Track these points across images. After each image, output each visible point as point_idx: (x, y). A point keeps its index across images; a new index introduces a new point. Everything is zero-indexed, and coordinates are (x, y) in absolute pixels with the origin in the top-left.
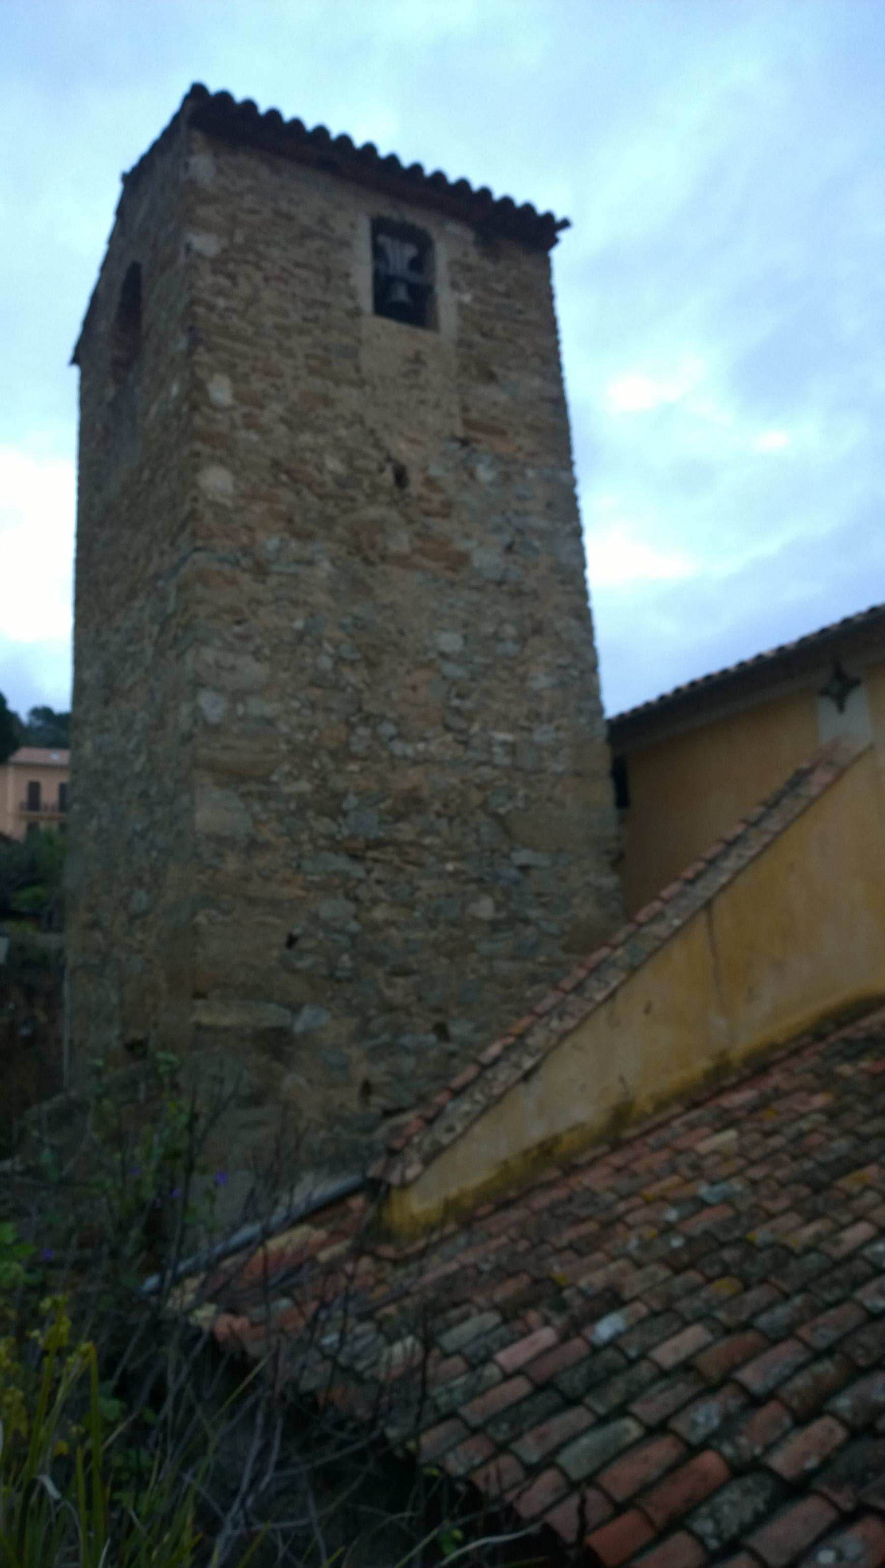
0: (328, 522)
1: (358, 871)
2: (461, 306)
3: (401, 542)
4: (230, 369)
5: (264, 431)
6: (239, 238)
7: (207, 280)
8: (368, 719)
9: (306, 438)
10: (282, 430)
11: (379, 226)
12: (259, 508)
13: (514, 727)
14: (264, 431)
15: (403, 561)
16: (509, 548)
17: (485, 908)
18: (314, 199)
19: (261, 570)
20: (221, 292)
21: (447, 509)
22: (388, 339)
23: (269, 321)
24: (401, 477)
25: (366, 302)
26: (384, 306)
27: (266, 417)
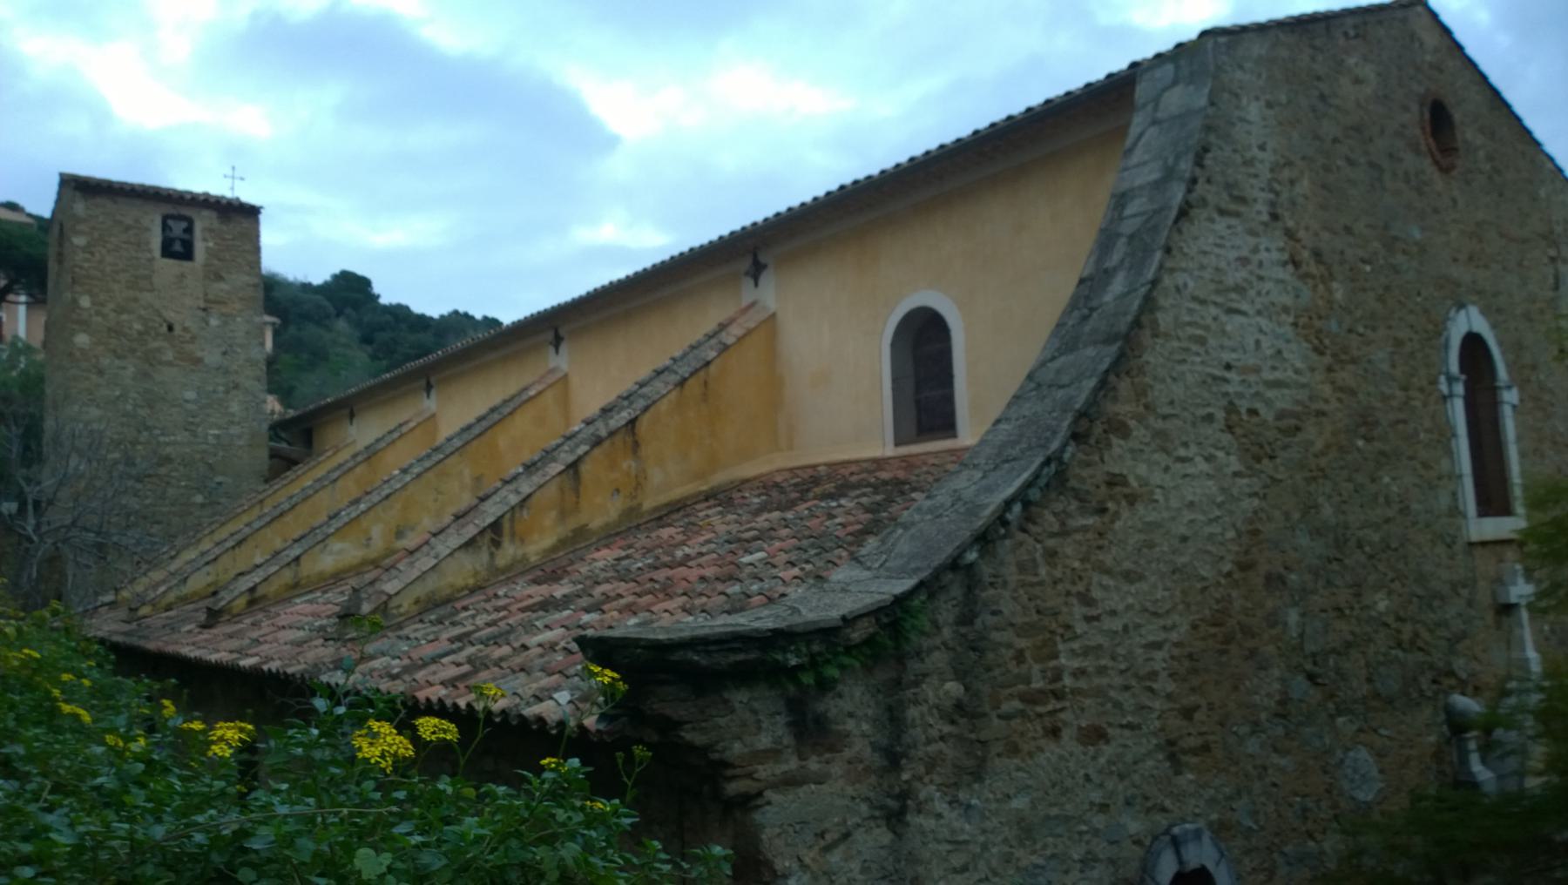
0: (133, 351)
1: (139, 486)
2: (207, 248)
3: (169, 355)
4: (90, 293)
5: (104, 316)
6: (96, 235)
7: (80, 256)
8: (147, 428)
9: (124, 317)
10: (112, 315)
11: (165, 219)
12: (101, 348)
13: (219, 428)
14: (104, 316)
15: (170, 364)
16: (225, 353)
17: (199, 499)
18: (130, 212)
19: (101, 372)
20: (87, 260)
21: (193, 339)
22: (171, 266)
23: (108, 269)
24: (170, 328)
25: (157, 252)
26: (167, 251)
27: (106, 310)
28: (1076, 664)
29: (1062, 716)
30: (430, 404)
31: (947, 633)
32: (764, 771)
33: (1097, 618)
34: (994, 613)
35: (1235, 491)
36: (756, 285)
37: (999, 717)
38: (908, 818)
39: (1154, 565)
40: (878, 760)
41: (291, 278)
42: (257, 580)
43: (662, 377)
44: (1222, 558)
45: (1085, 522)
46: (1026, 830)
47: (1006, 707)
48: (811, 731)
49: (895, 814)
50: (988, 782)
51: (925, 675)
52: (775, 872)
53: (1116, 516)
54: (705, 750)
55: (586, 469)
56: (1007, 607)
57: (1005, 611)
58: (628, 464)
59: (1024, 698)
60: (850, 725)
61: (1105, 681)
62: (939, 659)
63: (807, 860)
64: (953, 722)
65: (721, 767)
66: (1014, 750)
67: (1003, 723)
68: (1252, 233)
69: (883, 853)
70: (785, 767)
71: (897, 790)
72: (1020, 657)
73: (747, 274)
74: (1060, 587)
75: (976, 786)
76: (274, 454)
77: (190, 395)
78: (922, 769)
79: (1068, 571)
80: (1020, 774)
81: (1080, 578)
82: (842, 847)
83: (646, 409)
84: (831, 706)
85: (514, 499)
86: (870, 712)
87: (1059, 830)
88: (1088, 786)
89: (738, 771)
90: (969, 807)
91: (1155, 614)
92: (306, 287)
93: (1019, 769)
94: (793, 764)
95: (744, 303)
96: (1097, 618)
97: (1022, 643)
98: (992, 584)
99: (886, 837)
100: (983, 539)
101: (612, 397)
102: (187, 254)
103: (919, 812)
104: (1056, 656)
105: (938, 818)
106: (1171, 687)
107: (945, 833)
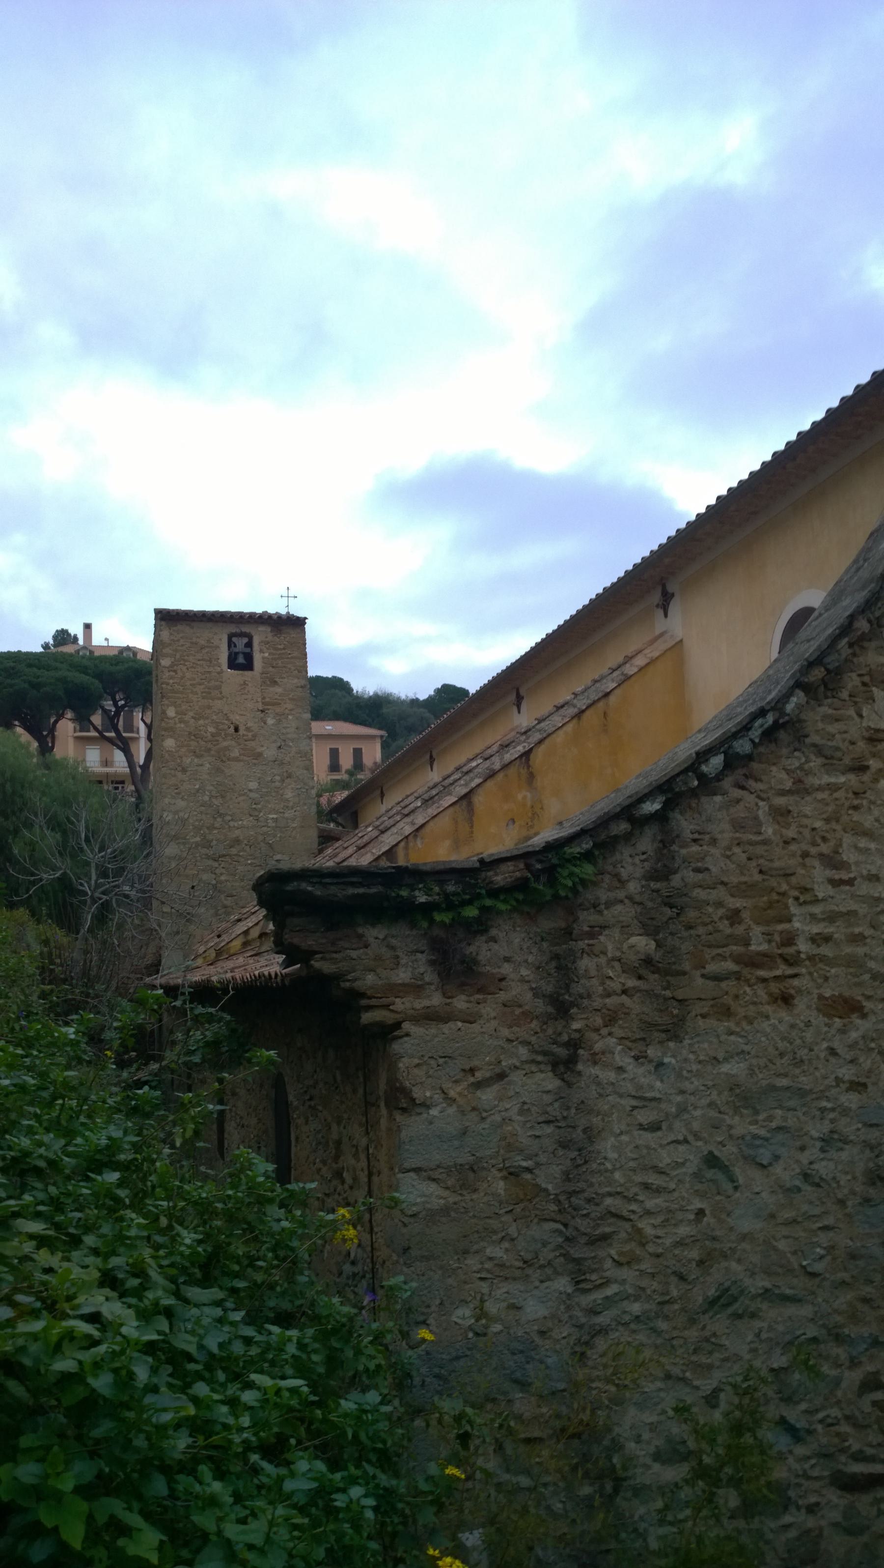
2: (263, 658)
6: (178, 656)
8: (221, 815)
9: (201, 722)
13: (277, 812)
15: (236, 759)
18: (203, 634)
19: (184, 771)
20: (171, 678)
23: (188, 683)
24: (236, 729)
27: (186, 718)
28: (815, 929)
29: (796, 982)
31: (633, 887)
32: (400, 1004)
33: (850, 882)
34: (698, 870)
36: (666, 615)
37: (703, 976)
38: (580, 1067)
40: (541, 1006)
41: (403, 697)
42: (250, 925)
43: (562, 711)
45: (833, 780)
46: (744, 1099)
47: (712, 968)
48: (457, 971)
49: (565, 1061)
50: (687, 1042)
51: (603, 927)
52: (414, 1100)
54: (337, 977)
55: (478, 800)
56: (716, 863)
57: (714, 869)
58: (523, 795)
59: (737, 959)
60: (506, 969)
61: (860, 950)
62: (624, 912)
63: (452, 1094)
64: (640, 978)
65: (354, 999)
69: (547, 1098)
70: (426, 1003)
71: (565, 1038)
72: (734, 917)
73: (657, 606)
74: (793, 847)
75: (671, 1044)
77: (253, 785)
78: (599, 1021)
79: (807, 833)
80: (732, 1038)
81: (824, 839)
82: (496, 1087)
83: (541, 742)
84: (482, 950)
85: (408, 830)
86: (531, 959)
87: (791, 1103)
88: (833, 1060)
89: (373, 1002)
90: (660, 1065)
92: (415, 702)
94: (436, 1000)
95: (657, 633)
97: (736, 903)
98: (695, 841)
99: (552, 1083)
103: (595, 1063)
105: (617, 1071)
107: (629, 1088)
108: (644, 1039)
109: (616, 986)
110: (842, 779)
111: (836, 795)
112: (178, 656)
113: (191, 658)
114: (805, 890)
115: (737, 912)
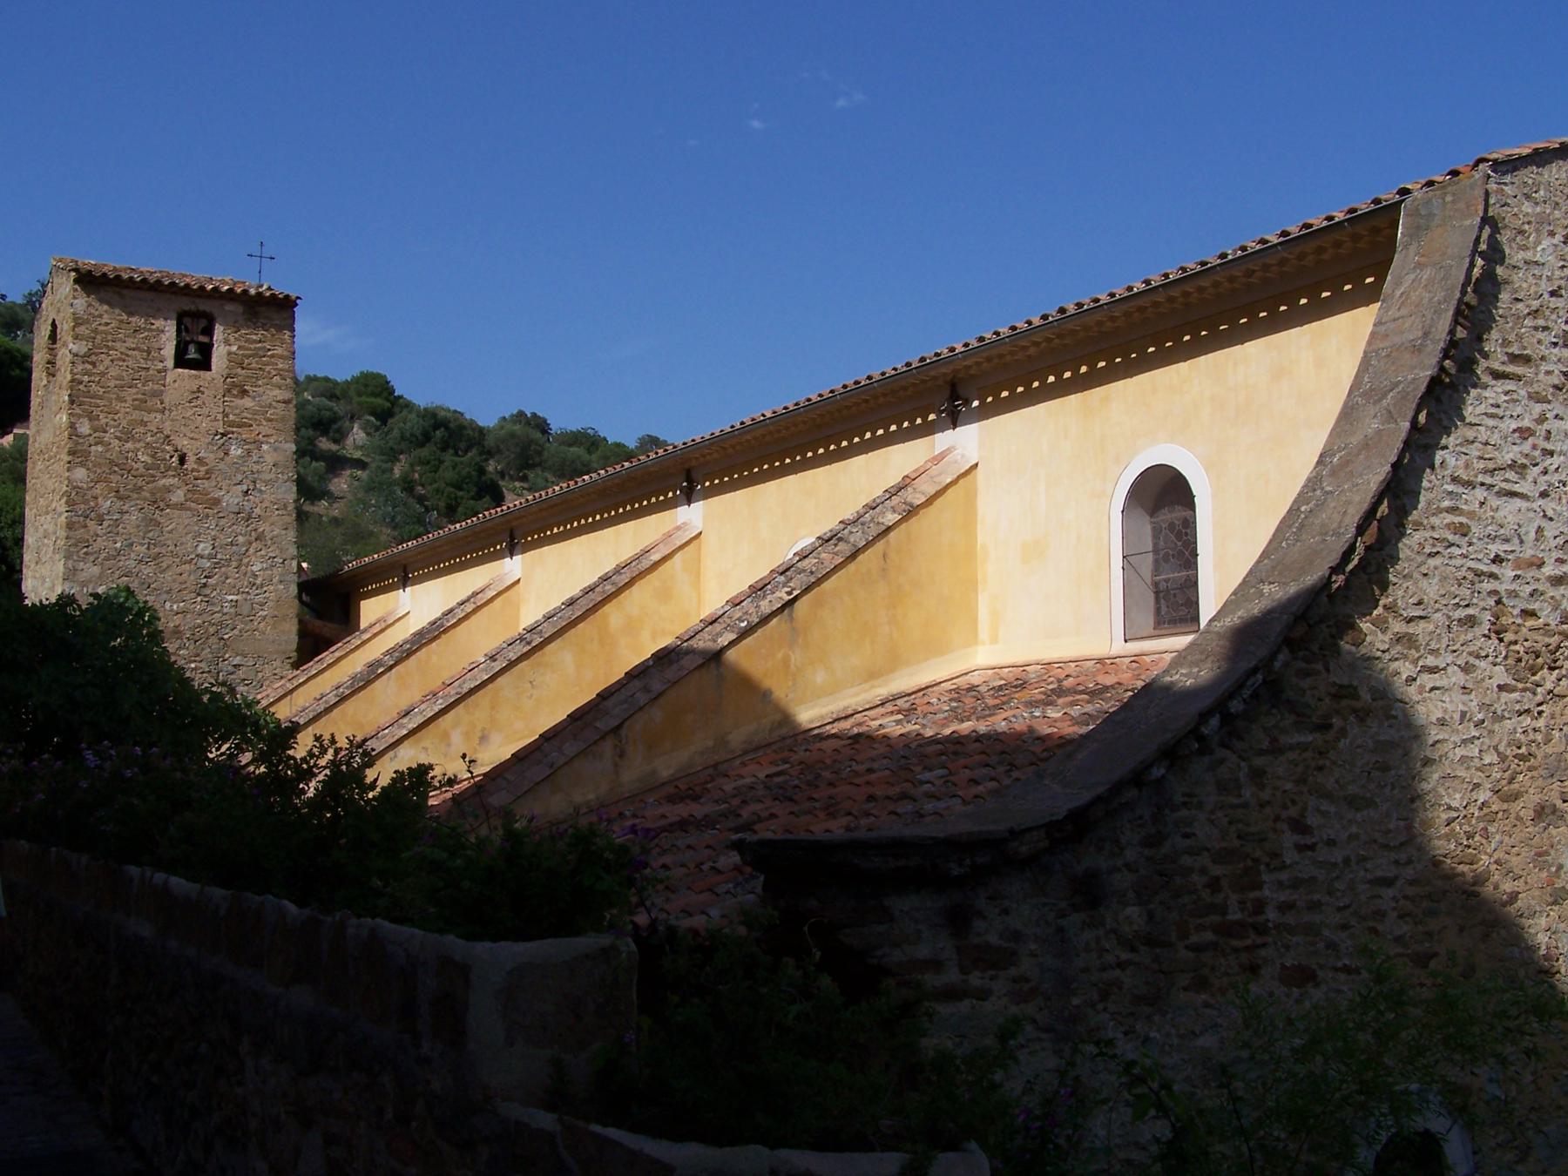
2: (229, 353)
9: (129, 445)
15: (181, 506)
23: (112, 384)
24: (182, 460)
25: (170, 363)
26: (181, 361)
27: (107, 438)
28: (1283, 896)
29: (1263, 953)
30: (512, 567)
31: (1130, 855)
33: (1312, 848)
34: (1186, 836)
35: (1499, 708)
37: (1187, 947)
39: (1387, 790)
44: (1477, 786)
45: (1302, 739)
50: (1169, 1016)
53: (1343, 732)
66: (1201, 984)
67: (1191, 955)
68: (1537, 398)
72: (1214, 885)
74: (1268, 810)
76: (304, 633)
77: (204, 548)
81: (1294, 802)
90: (1147, 1039)
91: (1386, 847)
93: (1207, 1005)
96: (1312, 848)
97: (1217, 870)
100: (1171, 754)
101: (761, 572)
102: (204, 364)
104: (1259, 886)
106: (1405, 928)
108: (1132, 1014)
109: (1110, 958)
110: (1310, 739)
111: (1305, 755)
112: (98, 341)
113: (118, 345)
114: (1275, 855)
115: (1217, 879)
